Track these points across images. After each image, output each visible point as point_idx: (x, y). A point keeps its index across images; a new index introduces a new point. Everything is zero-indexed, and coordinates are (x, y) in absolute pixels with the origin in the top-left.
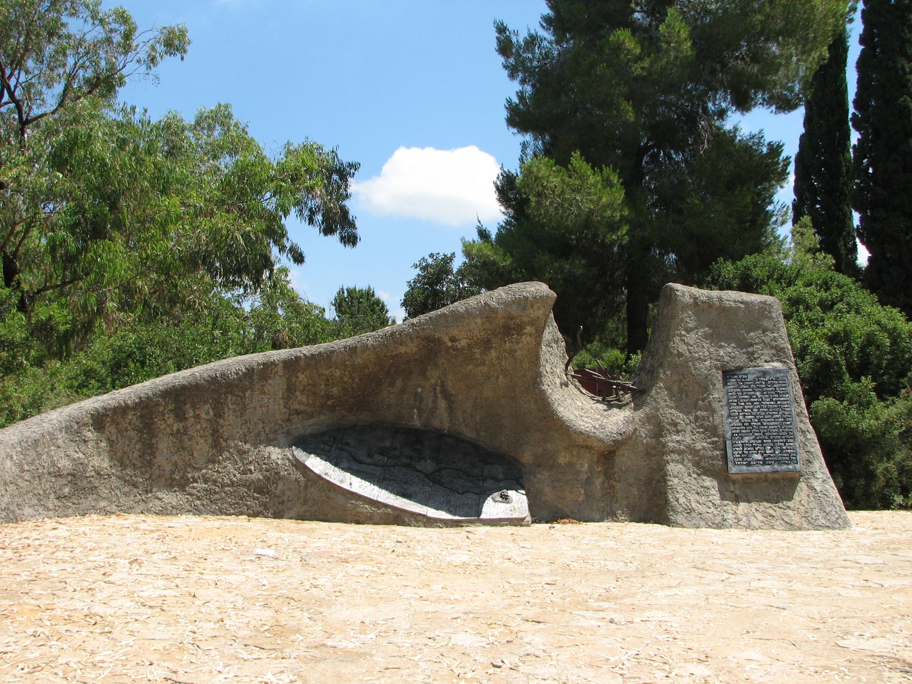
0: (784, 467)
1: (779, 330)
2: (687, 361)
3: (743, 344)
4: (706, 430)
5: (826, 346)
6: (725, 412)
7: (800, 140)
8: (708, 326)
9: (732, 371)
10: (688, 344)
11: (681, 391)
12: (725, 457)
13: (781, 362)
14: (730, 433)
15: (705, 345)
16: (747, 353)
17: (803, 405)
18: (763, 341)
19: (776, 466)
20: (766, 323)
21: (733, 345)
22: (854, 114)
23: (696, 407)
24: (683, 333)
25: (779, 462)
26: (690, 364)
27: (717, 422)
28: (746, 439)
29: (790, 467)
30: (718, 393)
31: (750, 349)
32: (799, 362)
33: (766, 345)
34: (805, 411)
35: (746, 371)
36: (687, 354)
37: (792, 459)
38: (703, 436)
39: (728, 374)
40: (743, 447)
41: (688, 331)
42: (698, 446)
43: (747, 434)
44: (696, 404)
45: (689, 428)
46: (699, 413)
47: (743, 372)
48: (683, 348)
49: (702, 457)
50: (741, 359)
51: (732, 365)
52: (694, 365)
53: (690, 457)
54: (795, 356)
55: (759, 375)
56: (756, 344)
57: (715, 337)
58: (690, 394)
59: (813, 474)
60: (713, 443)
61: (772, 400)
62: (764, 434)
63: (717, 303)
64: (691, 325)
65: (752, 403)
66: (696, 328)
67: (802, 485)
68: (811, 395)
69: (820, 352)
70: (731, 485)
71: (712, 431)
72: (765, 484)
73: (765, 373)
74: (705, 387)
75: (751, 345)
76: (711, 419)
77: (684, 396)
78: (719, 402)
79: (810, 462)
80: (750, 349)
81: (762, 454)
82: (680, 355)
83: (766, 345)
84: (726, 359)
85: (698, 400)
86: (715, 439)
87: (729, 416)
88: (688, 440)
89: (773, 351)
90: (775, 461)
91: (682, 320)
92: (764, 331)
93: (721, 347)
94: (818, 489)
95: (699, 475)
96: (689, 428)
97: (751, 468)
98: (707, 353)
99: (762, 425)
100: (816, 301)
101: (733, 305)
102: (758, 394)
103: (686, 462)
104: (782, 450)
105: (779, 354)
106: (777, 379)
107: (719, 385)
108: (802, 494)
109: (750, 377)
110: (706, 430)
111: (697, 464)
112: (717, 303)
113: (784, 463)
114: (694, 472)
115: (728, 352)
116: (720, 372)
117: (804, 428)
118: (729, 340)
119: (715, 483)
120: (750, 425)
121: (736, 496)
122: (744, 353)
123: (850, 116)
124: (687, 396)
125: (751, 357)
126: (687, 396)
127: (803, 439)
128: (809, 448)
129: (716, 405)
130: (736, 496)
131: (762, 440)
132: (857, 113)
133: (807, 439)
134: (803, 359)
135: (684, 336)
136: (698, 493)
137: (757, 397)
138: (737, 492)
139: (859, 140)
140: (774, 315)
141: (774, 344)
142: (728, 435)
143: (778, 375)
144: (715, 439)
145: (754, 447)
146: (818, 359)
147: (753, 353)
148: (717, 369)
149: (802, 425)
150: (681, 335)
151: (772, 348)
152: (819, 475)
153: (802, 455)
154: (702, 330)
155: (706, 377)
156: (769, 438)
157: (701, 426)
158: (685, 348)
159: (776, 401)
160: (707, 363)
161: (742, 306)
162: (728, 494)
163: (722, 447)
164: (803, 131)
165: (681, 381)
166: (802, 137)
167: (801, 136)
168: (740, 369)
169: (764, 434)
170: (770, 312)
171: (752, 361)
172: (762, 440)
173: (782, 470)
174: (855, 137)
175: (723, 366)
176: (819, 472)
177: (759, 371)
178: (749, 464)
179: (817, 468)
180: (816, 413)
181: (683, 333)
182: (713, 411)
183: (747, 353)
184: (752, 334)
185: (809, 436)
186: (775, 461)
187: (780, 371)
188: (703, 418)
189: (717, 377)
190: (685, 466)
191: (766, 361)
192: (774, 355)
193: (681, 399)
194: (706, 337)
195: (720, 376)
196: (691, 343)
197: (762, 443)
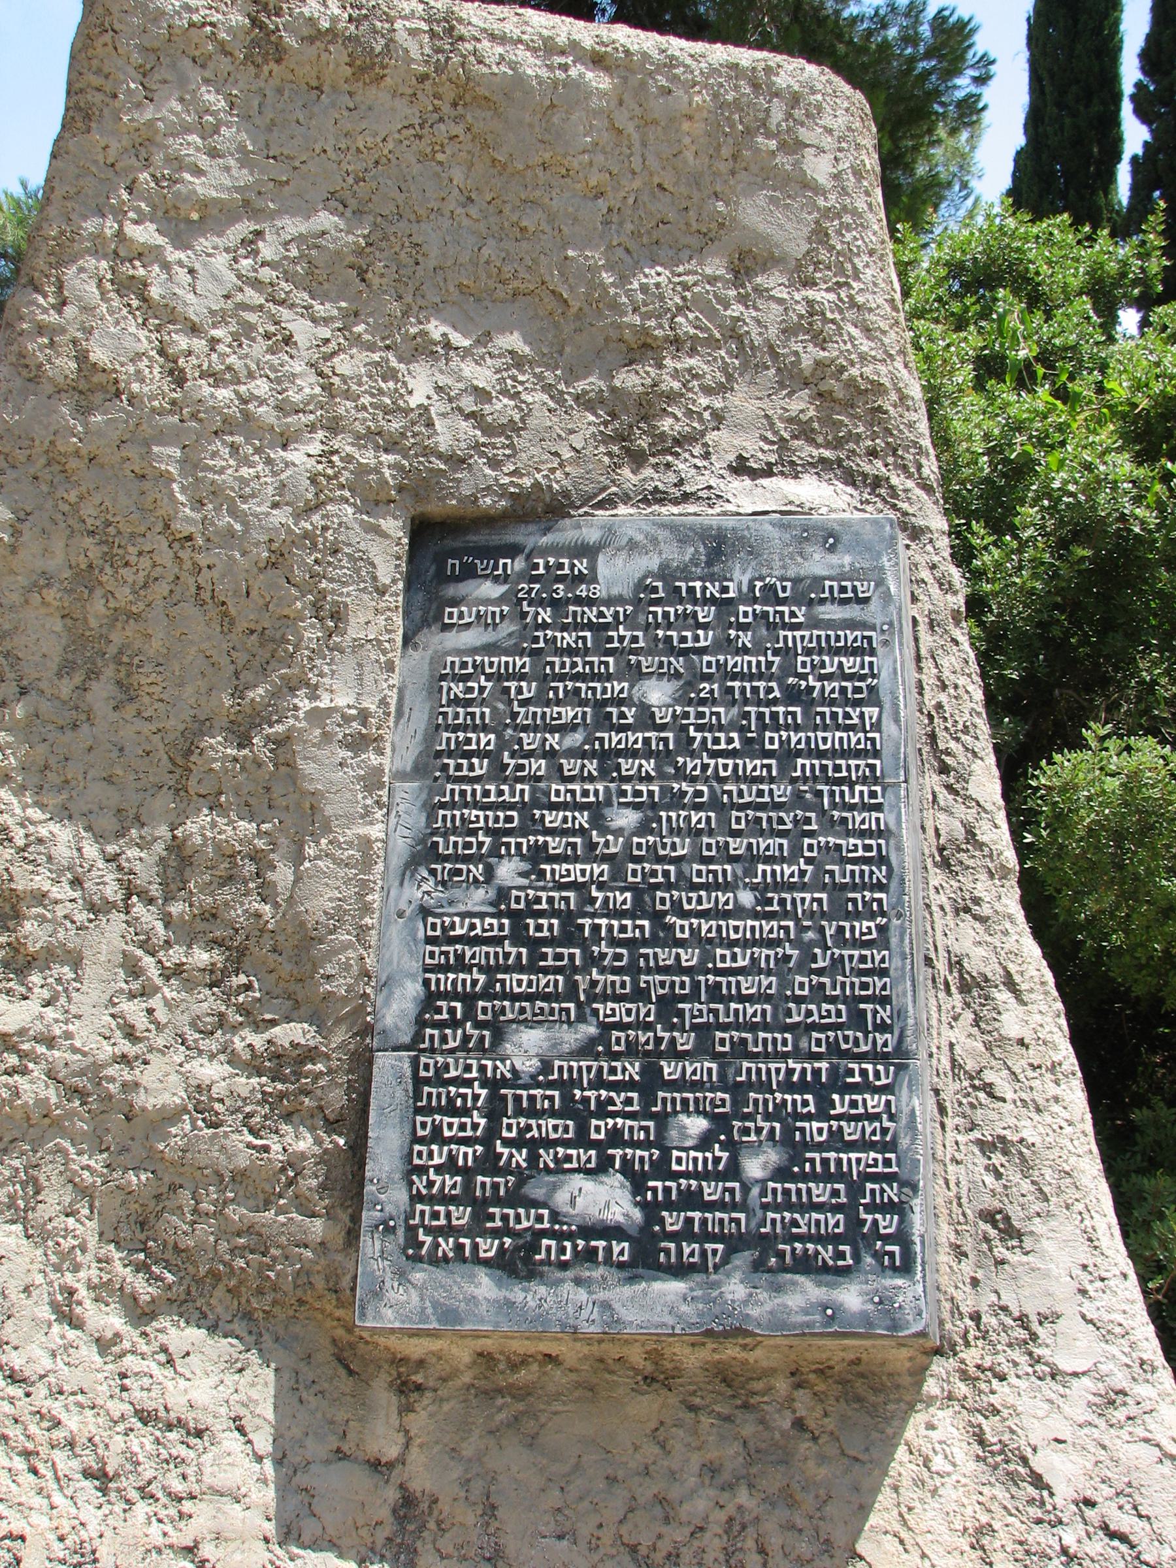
0: (804, 1293)
1: (844, 272)
2: (139, 438)
3: (581, 338)
4: (238, 958)
5: (1123, 466)
6: (392, 829)
7: (1016, 161)
8: (337, 201)
9: (490, 521)
10: (161, 315)
11: (83, 656)
12: (348, 1177)
13: (850, 478)
14: (413, 989)
15: (301, 329)
16: (610, 403)
17: (986, 783)
18: (733, 333)
19: (735, 1288)
20: (758, 215)
21: (513, 341)
22: (1139, 85)
23: (182, 775)
24: (144, 234)
25: (766, 1255)
26: (168, 456)
27: (320, 901)
28: (526, 1048)
29: (851, 1297)
30: (364, 677)
31: (630, 380)
32: (980, 534)
33: (748, 356)
34: (998, 835)
35: (589, 527)
36: (152, 383)
37: (870, 1228)
38: (207, 1002)
39: (444, 547)
40: (495, 1112)
41: (185, 222)
42: (161, 1084)
43: (537, 1007)
44: (186, 750)
45: (112, 935)
46: (199, 826)
47: (566, 533)
48: (122, 343)
49: (176, 1178)
50: (557, 442)
51: (483, 485)
52: (190, 464)
53: (90, 1165)
54: (955, 506)
55: (676, 555)
56: (676, 342)
57: (381, 281)
58: (144, 678)
59: (1028, 1329)
60: (280, 1063)
61: (752, 747)
62: (668, 1006)
63: (417, 49)
64: (212, 182)
65: (607, 758)
66: (248, 209)
67: (935, 1433)
68: (1037, 707)
69: (1092, 489)
70: (384, 1397)
71: (267, 964)
72: (647, 1407)
73: (719, 546)
74: (267, 630)
75: (643, 349)
76: (282, 875)
77: (101, 692)
78: (358, 744)
79: (1011, 1233)
80: (630, 380)
81: (637, 1181)
82: (94, 386)
83: (748, 356)
84: (451, 433)
85: (202, 726)
86: (293, 1033)
87: (425, 855)
88: (90, 1034)
89: (800, 404)
90: (735, 1243)
91: (144, 144)
92: (744, 266)
93: (421, 349)
94: (1065, 1472)
95: (141, 1314)
96: (112, 935)
97: (531, 1296)
98: (308, 387)
99: (664, 936)
100: (1076, 277)
101: (532, 67)
102: (657, 694)
103: (54, 1199)
104: (795, 1148)
105: (837, 422)
106: (807, 592)
107: (376, 618)
108: (928, 1517)
109: (615, 574)
110: (238, 958)
111: (136, 1229)
112: (417, 49)
113: (805, 1265)
114: (102, 1291)
115: (469, 394)
116: (394, 526)
117: (979, 961)
118: (481, 301)
119: (259, 1388)
120: (570, 935)
121: (407, 1505)
122: (586, 402)
123: (1128, 88)
124: (127, 692)
125: (636, 431)
126: (127, 692)
127: (969, 1046)
128: (1000, 1120)
129: (326, 770)
130: (407, 1505)
131: (651, 1060)
132: (1145, 81)
133: (995, 1044)
134: (1001, 525)
135: (145, 254)
136: (101, 1477)
137: (646, 718)
138: (421, 1475)
139: (1146, 144)
140: (819, 168)
141: (810, 355)
142: (398, 1009)
143: (818, 563)
144: (293, 1033)
145: (579, 1113)
146: (1076, 527)
147: (648, 405)
148: (373, 501)
149: (965, 939)
150: (122, 251)
151: (792, 378)
152: (1072, 1348)
153: (948, 1179)
154: (293, 226)
155: (278, 559)
156: (705, 1048)
157: (204, 926)
158: (144, 341)
159: (788, 755)
160: (301, 457)
161: (598, 81)
162: (342, 1486)
163: (337, 1099)
164: (1020, 140)
165: (85, 579)
166: (1020, 156)
167: (1018, 153)
168: (549, 508)
169: (668, 1006)
170: (795, 146)
171: (638, 459)
172: (651, 1060)
173: (778, 1323)
174: (1135, 135)
175: (415, 486)
176: (1070, 1324)
177: (681, 534)
178: (518, 1263)
179: (1063, 1289)
180: (1060, 820)
181: (144, 234)
182: (307, 819)
183: (610, 403)
184: (656, 276)
185: (1012, 1023)
186: (735, 1243)
187: (831, 538)
188: (228, 867)
189: (361, 561)
190: (38, 1234)
191: (740, 468)
192: (805, 432)
193: (78, 716)
194: (314, 272)
195: (385, 550)
196: (195, 307)
197: (651, 1082)
